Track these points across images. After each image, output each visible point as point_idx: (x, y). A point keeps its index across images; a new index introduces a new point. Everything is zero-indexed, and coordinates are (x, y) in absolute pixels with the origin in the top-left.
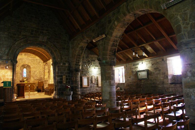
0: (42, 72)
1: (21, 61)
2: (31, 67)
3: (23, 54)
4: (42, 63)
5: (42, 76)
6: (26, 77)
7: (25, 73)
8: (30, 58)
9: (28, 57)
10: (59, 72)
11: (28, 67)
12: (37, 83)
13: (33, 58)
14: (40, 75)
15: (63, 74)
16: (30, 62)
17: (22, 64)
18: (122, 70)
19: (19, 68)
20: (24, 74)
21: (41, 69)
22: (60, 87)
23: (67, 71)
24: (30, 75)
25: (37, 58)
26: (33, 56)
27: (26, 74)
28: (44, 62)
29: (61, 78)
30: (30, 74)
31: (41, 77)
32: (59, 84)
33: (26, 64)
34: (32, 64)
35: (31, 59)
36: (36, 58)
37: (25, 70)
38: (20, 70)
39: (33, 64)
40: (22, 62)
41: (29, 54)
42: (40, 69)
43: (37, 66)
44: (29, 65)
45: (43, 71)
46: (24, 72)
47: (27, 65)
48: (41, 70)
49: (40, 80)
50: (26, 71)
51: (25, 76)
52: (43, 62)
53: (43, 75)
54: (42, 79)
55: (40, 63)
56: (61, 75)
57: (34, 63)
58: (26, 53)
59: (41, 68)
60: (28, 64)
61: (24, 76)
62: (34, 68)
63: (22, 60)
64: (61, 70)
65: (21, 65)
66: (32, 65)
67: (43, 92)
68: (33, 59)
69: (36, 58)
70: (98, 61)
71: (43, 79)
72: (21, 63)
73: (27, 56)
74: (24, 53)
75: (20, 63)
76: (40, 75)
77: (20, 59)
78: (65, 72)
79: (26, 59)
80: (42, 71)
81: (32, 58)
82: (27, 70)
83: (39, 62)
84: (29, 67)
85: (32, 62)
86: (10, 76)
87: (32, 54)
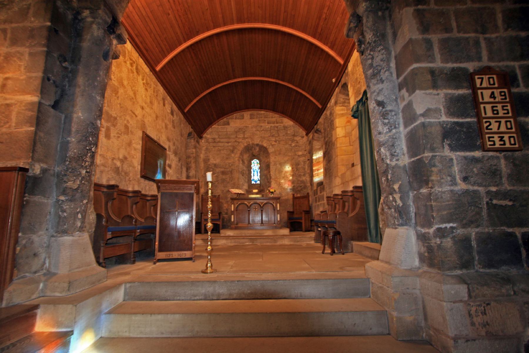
0: (304, 165)
1: (241, 136)
2: (271, 150)
3: (247, 114)
4: (303, 137)
5: (304, 178)
6: (258, 182)
7: (256, 173)
8: (266, 124)
9: (259, 123)
10: (428, 42)
11: (262, 153)
12: (291, 202)
13: (274, 123)
14: (300, 176)
15: (469, 59)
16: (268, 136)
17: (246, 145)
18: (197, 272)
19: (238, 155)
20: (252, 175)
21: (299, 156)
22: (462, 186)
23: (512, 33)
24: (269, 176)
25: (286, 124)
26: (274, 119)
27: (259, 174)
28: (307, 134)
29: (460, 99)
30: (269, 172)
31: (303, 182)
32: (447, 152)
33: (255, 143)
34: (274, 143)
35: (268, 126)
36: (282, 123)
37: (255, 165)
38: (241, 162)
39: (276, 142)
40: (244, 138)
41: (263, 112)
42: (297, 157)
43: (287, 146)
44: (265, 145)
45: (308, 162)
46: (252, 170)
47: (257, 145)
48: (302, 159)
49: (299, 191)
50: (259, 165)
51: (256, 182)
52: (304, 133)
53: (307, 175)
54: (305, 187)
55: (296, 138)
56: (450, 65)
57: (277, 139)
58: (255, 112)
59: (300, 153)
60: (260, 143)
61: (253, 182)
62: (280, 154)
63: (244, 132)
64: (448, 29)
65: (243, 146)
66: (272, 145)
67: (308, 230)
68: (275, 127)
69: (282, 123)
70: (394, 188)
71: (310, 188)
72: (240, 140)
73: (257, 120)
74: (250, 113)
75: (239, 142)
76: (300, 176)
77: (240, 129)
78: (489, 41)
79: (254, 129)
80: (304, 162)
81: (272, 125)
82: (260, 162)
83: (294, 136)
84: (264, 152)
85: (273, 136)
86: (24, 92)
87: (270, 114)
